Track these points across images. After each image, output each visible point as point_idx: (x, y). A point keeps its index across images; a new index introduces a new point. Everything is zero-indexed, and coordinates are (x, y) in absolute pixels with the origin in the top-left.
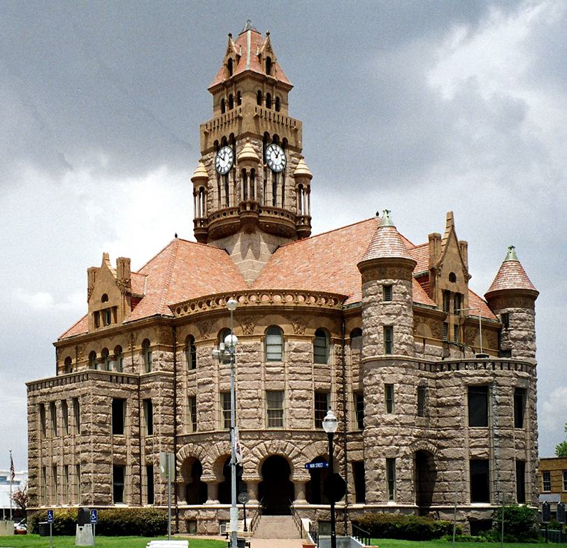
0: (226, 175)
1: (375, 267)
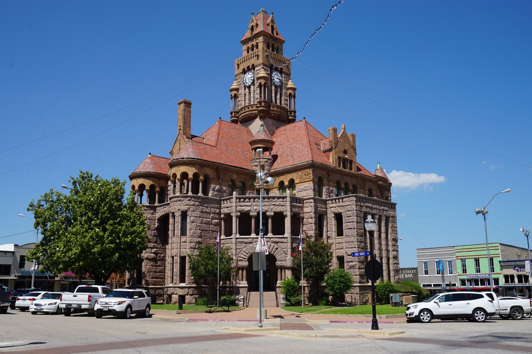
0: (249, 87)
1: (245, 174)
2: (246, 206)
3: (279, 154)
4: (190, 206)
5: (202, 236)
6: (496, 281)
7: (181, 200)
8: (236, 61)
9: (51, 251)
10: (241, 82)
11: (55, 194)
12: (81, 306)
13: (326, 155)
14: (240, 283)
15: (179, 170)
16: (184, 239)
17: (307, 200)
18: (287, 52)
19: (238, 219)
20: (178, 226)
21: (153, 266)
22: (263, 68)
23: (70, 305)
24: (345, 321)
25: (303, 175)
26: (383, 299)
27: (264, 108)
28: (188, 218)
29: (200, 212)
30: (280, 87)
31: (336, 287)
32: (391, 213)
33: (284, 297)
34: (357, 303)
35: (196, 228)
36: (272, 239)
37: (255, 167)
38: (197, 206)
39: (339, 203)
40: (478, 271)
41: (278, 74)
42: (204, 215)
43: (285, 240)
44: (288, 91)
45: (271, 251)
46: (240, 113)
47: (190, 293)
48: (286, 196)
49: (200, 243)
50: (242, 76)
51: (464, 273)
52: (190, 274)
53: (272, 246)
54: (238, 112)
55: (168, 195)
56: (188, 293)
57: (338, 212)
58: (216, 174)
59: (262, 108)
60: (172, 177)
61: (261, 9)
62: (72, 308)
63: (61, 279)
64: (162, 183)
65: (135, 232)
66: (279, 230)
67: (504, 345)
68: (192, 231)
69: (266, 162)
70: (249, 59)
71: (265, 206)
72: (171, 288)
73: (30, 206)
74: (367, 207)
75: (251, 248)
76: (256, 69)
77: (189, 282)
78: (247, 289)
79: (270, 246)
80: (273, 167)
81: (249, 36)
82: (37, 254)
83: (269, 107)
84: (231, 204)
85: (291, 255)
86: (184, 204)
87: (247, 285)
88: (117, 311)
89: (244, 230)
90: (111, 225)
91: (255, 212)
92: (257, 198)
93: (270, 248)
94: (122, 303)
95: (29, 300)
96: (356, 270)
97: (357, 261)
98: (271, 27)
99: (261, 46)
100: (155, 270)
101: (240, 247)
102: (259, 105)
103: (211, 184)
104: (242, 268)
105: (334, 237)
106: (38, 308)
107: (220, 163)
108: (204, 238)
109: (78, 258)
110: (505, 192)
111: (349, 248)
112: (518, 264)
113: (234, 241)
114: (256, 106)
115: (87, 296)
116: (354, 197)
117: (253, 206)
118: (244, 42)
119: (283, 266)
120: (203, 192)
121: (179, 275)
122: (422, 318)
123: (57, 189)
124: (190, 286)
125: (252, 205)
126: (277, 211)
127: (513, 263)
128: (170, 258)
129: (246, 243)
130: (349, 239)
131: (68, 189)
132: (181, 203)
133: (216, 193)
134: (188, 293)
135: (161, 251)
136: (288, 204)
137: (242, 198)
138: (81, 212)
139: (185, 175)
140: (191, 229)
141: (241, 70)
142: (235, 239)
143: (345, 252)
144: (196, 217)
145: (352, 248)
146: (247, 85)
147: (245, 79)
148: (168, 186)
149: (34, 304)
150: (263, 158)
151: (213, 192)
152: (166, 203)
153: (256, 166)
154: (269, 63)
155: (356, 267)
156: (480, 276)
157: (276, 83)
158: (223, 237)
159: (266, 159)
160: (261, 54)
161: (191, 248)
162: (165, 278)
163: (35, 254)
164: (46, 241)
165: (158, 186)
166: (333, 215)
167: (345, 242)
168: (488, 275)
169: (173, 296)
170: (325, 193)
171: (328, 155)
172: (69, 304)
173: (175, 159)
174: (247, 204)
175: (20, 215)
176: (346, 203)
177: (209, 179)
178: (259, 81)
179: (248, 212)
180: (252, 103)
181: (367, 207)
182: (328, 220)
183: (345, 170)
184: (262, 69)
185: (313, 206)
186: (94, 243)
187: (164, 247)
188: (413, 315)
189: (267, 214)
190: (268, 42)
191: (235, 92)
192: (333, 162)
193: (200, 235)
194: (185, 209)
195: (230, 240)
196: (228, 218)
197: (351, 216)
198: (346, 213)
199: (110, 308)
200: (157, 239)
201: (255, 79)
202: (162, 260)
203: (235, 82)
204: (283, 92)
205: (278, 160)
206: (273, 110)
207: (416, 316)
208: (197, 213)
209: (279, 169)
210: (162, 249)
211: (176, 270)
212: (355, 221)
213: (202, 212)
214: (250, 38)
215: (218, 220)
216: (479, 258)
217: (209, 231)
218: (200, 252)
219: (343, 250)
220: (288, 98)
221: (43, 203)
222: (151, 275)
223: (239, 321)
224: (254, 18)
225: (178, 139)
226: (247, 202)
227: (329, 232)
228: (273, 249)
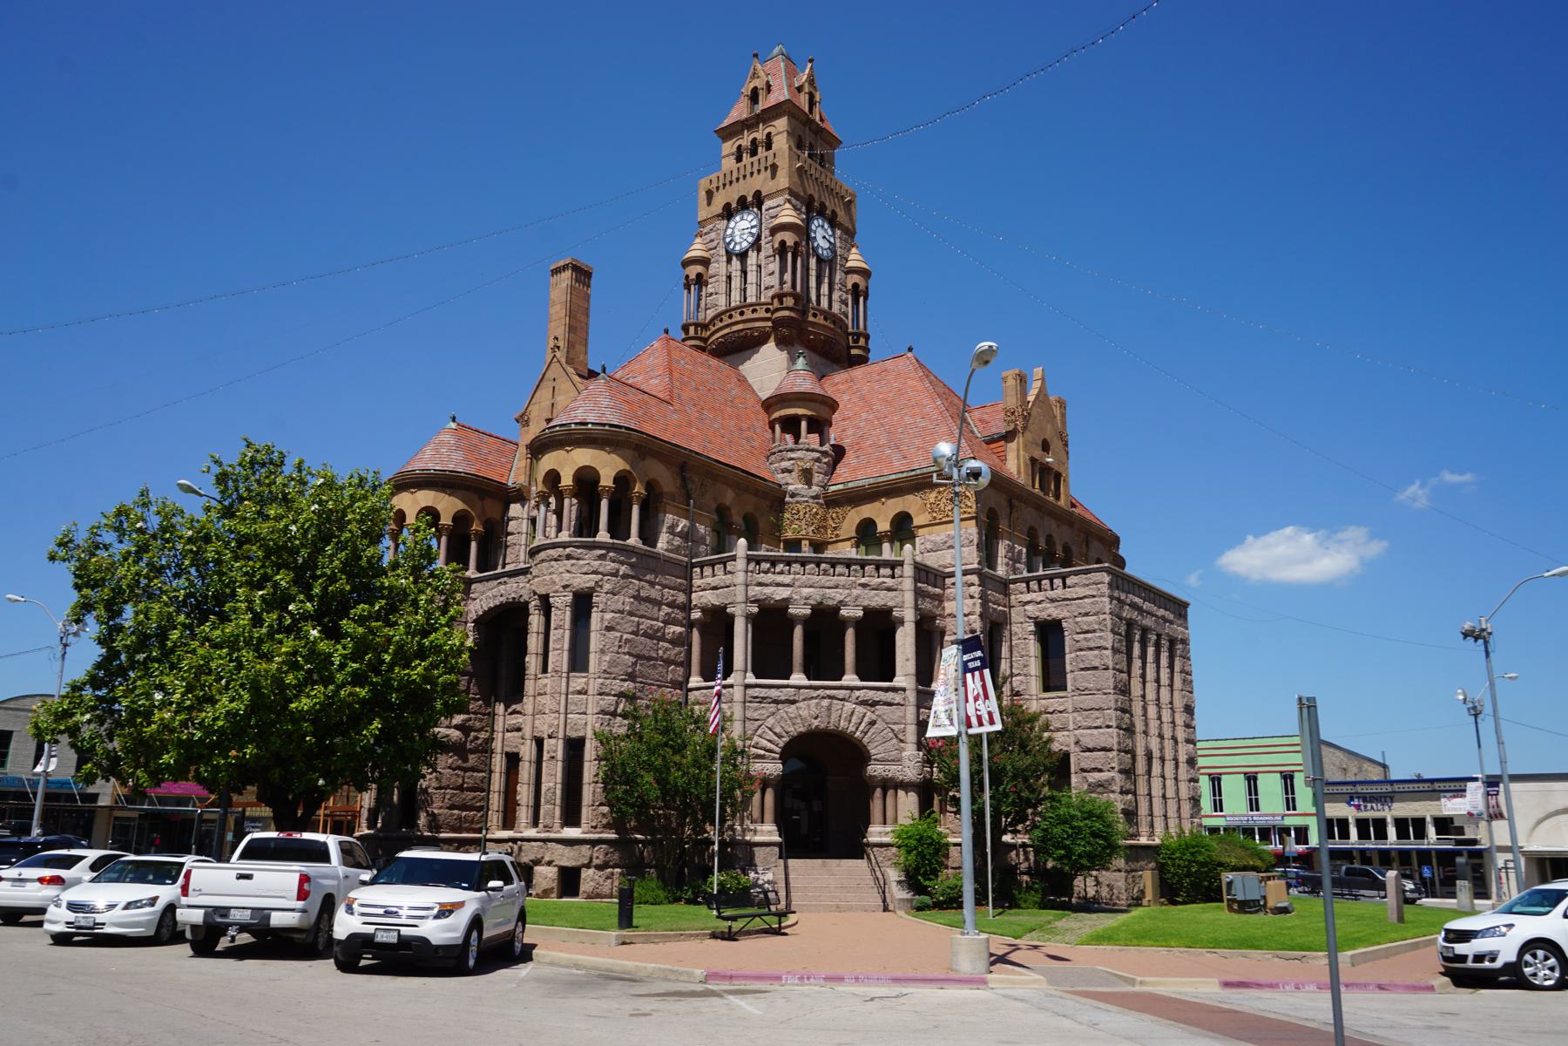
0: (743, 256)
1: (756, 493)
2: (778, 585)
3: (846, 443)
4: (604, 575)
5: (636, 677)
6: (1302, 835)
7: (576, 555)
8: (704, 184)
9: (133, 702)
10: (716, 242)
11: (154, 509)
12: (269, 917)
13: (995, 451)
14: (755, 831)
15: (566, 463)
16: (578, 682)
18: (846, 171)
19: (749, 626)
20: (561, 638)
21: (454, 770)
22: (789, 201)
23: (222, 912)
24: (1274, 982)
25: (944, 500)
26: (1182, 886)
27: (793, 314)
29: (634, 597)
30: (827, 264)
31: (1079, 850)
32: (1176, 631)
33: (903, 878)
34: (1118, 898)
35: (620, 647)
36: (857, 693)
37: (782, 475)
38: (625, 576)
39: (1052, 589)
40: (1254, 805)
41: (826, 226)
42: (644, 608)
43: (897, 698)
44: (849, 276)
45: (854, 729)
46: (713, 329)
47: (596, 862)
48: (901, 559)
49: (631, 698)
50: (722, 224)
51: (1216, 811)
52: (601, 797)
53: (856, 713)
54: (705, 327)
55: (507, 547)
56: (591, 859)
57: (1049, 618)
58: (679, 482)
59: (786, 313)
60: (544, 482)
61: (776, 50)
62: (231, 925)
63: (116, 802)
64: (492, 509)
65: (437, 649)
66: (878, 665)
68: (607, 658)
69: (818, 460)
70: (745, 177)
71: (836, 587)
72: (533, 843)
73: (59, 545)
74: (1133, 606)
76: (767, 204)
77: (594, 824)
80: (836, 478)
81: (745, 116)
82: (73, 715)
83: (804, 313)
84: (729, 576)
86: (585, 570)
87: (777, 839)
88: (434, 942)
89: (770, 662)
90: (361, 620)
91: (805, 604)
92: (811, 562)
93: (850, 721)
94: (451, 912)
95: (38, 884)
96: (1112, 795)
97: (1116, 769)
98: (807, 96)
99: (781, 143)
100: (460, 781)
101: (755, 715)
102: (776, 304)
103: (665, 513)
105: (1034, 692)
106: (82, 919)
107: (691, 451)
108: (641, 682)
109: (237, 730)
110: (1554, 575)
111: (1090, 728)
112: (1360, 791)
113: (738, 693)
114: (765, 307)
115: (295, 879)
116: (1105, 574)
117: (800, 587)
118: (728, 133)
119: (892, 779)
120: (641, 535)
121: (562, 799)
122: (1528, 970)
123: (165, 492)
124: (596, 836)
125: (797, 583)
126: (873, 604)
127: (1345, 789)
128: (528, 742)
129: (776, 702)
130: (1088, 701)
131: (201, 495)
132: (573, 565)
133: (677, 541)
134: (591, 859)
135: (481, 720)
136: (908, 584)
137: (766, 561)
138: (247, 573)
139: (586, 482)
140: (602, 652)
141: (718, 206)
142: (742, 688)
143: (1072, 740)
144: (621, 612)
145: (1100, 727)
146: (738, 248)
147: (729, 232)
148: (509, 520)
149: (64, 905)
150: (808, 450)
151: (671, 537)
152: (499, 570)
153: (785, 471)
154: (805, 192)
155: (1114, 788)
156: (1259, 819)
157: (820, 251)
158: (695, 681)
159: (817, 451)
160: (783, 164)
161: (603, 712)
162: (491, 807)
163: (67, 714)
164: (107, 672)
165: (479, 518)
166: (1032, 628)
167: (1075, 710)
168: (1280, 818)
169: (537, 869)
170: (1005, 560)
171: (1000, 450)
172: (217, 909)
173: (555, 426)
174: (780, 579)
175: (9, 596)
176: (1077, 589)
177: (661, 495)
178: (780, 236)
179: (784, 604)
180: (751, 299)
181: (1133, 606)
182: (1014, 643)
183: (1047, 497)
184: (788, 205)
185: (977, 595)
186: (298, 679)
187: (490, 710)
188: (1493, 960)
189: (844, 612)
190: (799, 136)
191: (699, 269)
192: (1019, 472)
193: (630, 670)
194: (588, 585)
196: (718, 624)
197: (1094, 631)
198: (1078, 619)
199: (405, 931)
200: (469, 682)
201: (765, 233)
202: (481, 752)
203: (698, 240)
204: (837, 280)
205: (849, 458)
206: (814, 324)
207: (1507, 965)
208: (624, 601)
209: (860, 483)
210: (484, 715)
211: (551, 785)
212: (1109, 646)
213: (637, 597)
214: (747, 120)
215: (682, 626)
216: (1256, 773)
217: (656, 659)
218: (631, 727)
219: (1066, 733)
220: (850, 297)
221: (109, 537)
222: (448, 796)
223: (896, 980)
224: (759, 67)
225: (547, 375)
226: (782, 573)
227: (1018, 678)
228: (860, 723)
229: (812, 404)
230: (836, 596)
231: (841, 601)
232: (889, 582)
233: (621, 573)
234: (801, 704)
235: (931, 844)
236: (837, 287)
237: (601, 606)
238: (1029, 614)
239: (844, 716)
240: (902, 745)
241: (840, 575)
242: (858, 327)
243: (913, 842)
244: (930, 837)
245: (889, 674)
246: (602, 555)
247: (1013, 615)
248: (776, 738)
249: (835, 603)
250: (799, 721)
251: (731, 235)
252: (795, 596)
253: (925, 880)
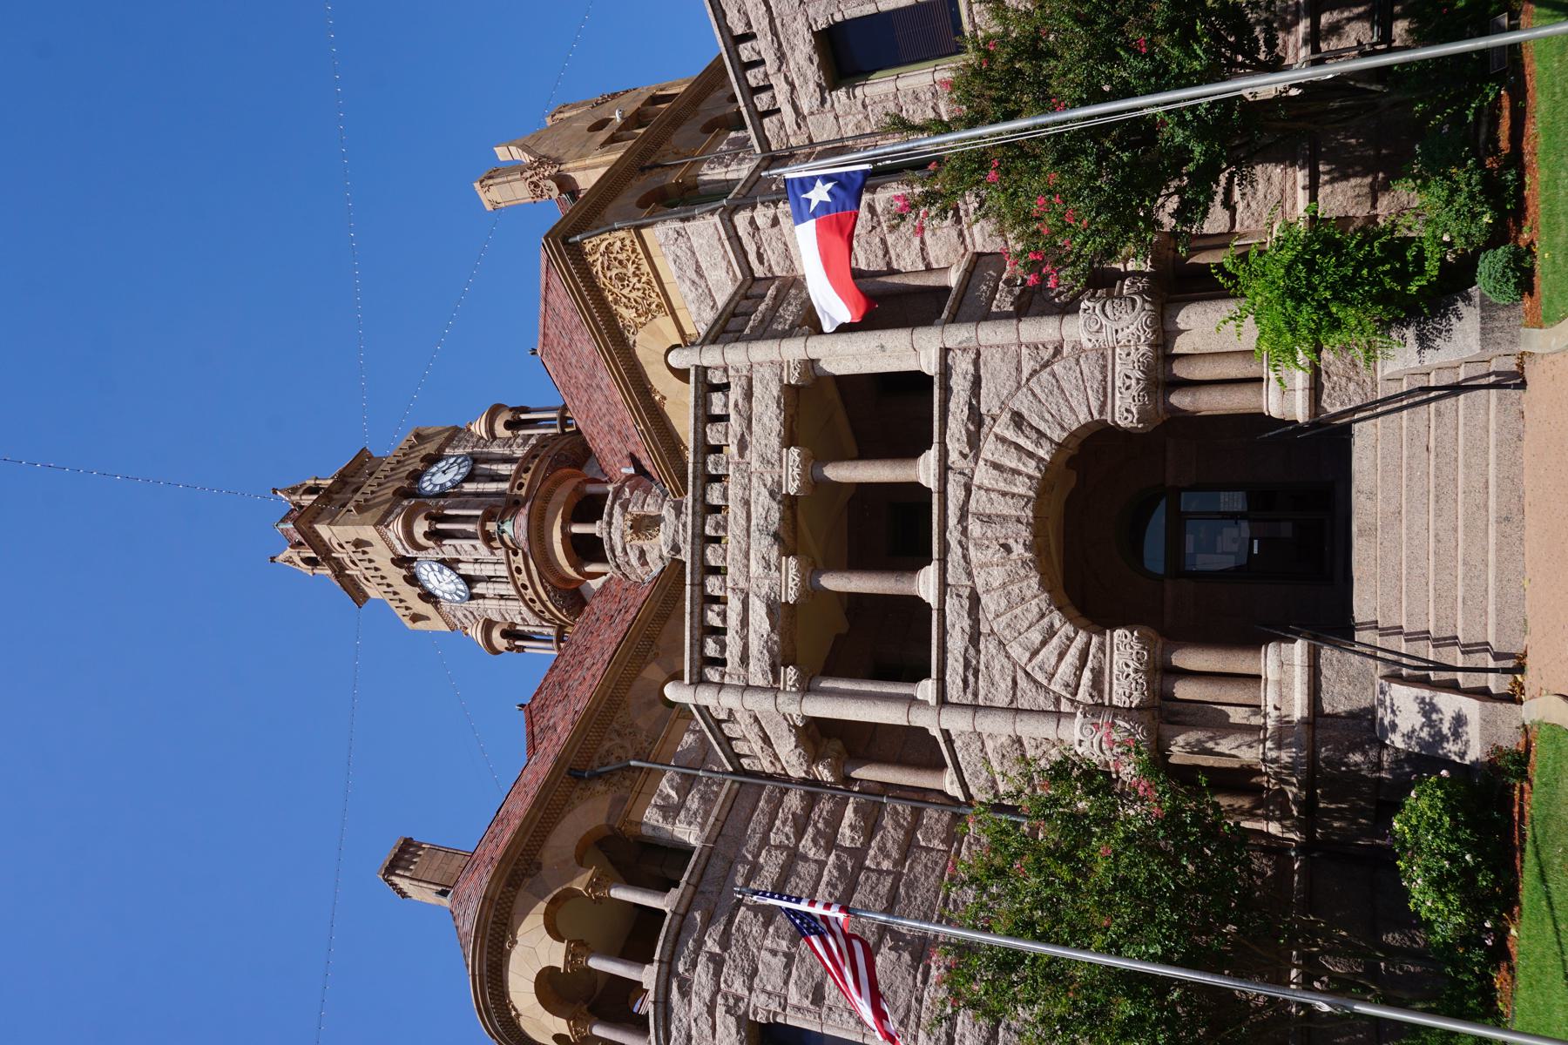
0: (469, 580)
2: (745, 622)
17: (745, 254)
19: (827, 684)
28: (794, 1020)
33: (1410, 333)
36: (954, 457)
38: (725, 943)
39: (762, 62)
43: (962, 366)
45: (1033, 463)
50: (445, 606)
53: (996, 458)
57: (816, 59)
58: (600, 787)
67: (1355, 175)
69: (624, 507)
71: (747, 503)
75: (1010, 607)
78: (1326, 652)
79: (997, 466)
85: (1067, 319)
86: (707, 1031)
91: (779, 569)
101: (1004, 685)
103: (641, 823)
104: (1161, 673)
113: (957, 723)
114: (511, 556)
117: (748, 579)
125: (742, 584)
126: (776, 426)
129: (974, 638)
146: (461, 587)
147: (447, 596)
151: (683, 813)
180: (502, 570)
185: (771, 212)
189: (792, 488)
193: (906, 957)
194: (733, 1031)
195: (958, 744)
217: (898, 877)
220: (521, 432)
226: (723, 616)
228: (1018, 447)
229: (548, 515)
230: (765, 510)
231: (772, 494)
232: (735, 393)
233: (717, 950)
234: (980, 583)
235: (1311, 266)
236: (507, 451)
237: (774, 1006)
238: (816, 103)
239: (1002, 486)
240: (1066, 350)
241: (725, 497)
242: (554, 419)
243: (1306, 314)
244: (1289, 269)
245: (918, 382)
246: (679, 988)
247: (825, 138)
248: (1055, 641)
249: (775, 505)
250: (1015, 589)
251: (451, 594)
252: (765, 590)
253: (1421, 271)
